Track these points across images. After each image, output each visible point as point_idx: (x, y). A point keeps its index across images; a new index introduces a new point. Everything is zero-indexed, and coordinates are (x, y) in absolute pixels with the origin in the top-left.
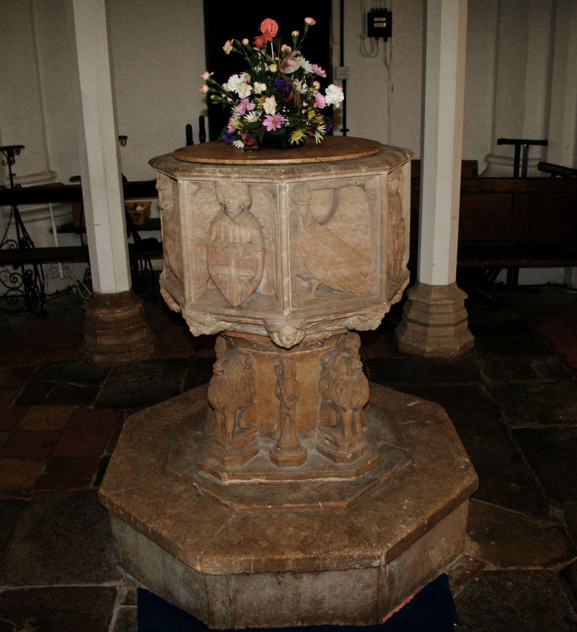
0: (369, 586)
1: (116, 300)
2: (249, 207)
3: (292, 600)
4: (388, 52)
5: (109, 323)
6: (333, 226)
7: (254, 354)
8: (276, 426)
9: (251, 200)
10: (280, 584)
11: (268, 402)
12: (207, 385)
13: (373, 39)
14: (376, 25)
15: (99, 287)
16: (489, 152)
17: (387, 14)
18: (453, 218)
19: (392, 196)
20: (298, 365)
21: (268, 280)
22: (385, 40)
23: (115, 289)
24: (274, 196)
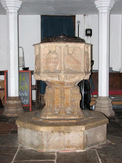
0: (81, 137)
1: (15, 98)
2: (55, 51)
3: (63, 141)
4: (91, 40)
5: (12, 105)
6: (73, 55)
7: (55, 87)
8: (60, 105)
9: (56, 49)
10: (60, 136)
11: (58, 99)
12: (40, 111)
13: (87, 36)
14: (88, 33)
15: (10, 95)
16: (120, 68)
17: (91, 30)
18: (107, 78)
19: (86, 53)
20: (65, 90)
21: (59, 66)
22: (90, 37)
23: (15, 95)
24: (61, 48)
